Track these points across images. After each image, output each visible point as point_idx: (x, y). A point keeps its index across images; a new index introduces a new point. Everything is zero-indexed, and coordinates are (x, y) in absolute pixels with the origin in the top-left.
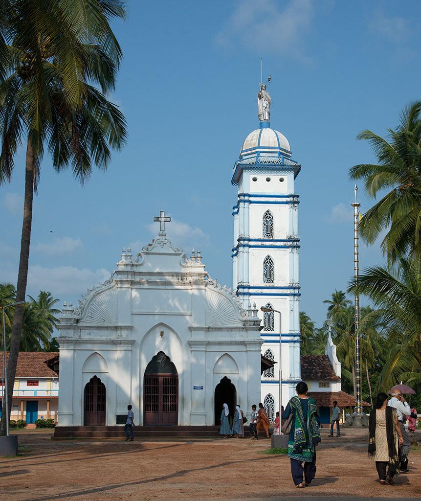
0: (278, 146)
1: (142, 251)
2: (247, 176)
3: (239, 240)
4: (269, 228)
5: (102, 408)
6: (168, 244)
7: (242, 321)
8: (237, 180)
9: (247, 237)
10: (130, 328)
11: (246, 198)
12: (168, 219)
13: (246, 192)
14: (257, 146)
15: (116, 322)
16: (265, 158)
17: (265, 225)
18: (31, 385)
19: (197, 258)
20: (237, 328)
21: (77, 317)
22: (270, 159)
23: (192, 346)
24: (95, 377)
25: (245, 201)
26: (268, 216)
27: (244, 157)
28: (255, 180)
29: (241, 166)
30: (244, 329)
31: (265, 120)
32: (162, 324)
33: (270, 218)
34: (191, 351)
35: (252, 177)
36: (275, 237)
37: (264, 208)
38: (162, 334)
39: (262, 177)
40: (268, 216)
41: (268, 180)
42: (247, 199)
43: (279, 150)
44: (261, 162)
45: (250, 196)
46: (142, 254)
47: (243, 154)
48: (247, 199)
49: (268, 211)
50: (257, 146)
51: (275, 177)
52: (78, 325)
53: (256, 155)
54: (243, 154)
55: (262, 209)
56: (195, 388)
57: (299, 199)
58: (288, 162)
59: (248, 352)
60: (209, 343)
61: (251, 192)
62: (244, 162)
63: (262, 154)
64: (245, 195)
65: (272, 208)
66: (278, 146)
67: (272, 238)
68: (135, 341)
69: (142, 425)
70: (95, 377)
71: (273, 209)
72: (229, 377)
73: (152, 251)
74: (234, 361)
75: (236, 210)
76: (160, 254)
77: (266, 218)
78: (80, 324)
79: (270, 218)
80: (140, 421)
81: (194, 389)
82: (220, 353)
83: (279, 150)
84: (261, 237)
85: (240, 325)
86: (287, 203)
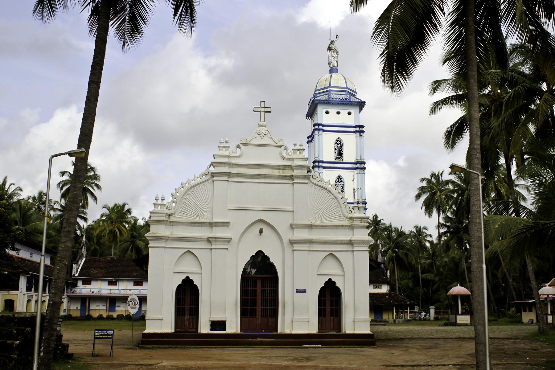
0: (345, 86)
1: (241, 142)
2: (321, 110)
3: (314, 162)
4: (339, 153)
5: (195, 312)
6: (268, 135)
7: (347, 218)
8: (311, 114)
9: (321, 159)
10: (226, 225)
11: (321, 127)
12: (269, 110)
13: (319, 122)
14: (329, 86)
15: (212, 218)
16: (334, 96)
17: (336, 150)
18: (111, 285)
19: (347, 95)
20: (342, 226)
21: (168, 212)
22: (340, 96)
23: (294, 245)
24: (188, 277)
25: (319, 130)
26: (339, 142)
27: (318, 95)
28: (327, 113)
29: (316, 101)
30: (351, 227)
31: (334, 67)
32: (261, 221)
33: (340, 144)
34: (293, 250)
35: (324, 110)
36: (345, 160)
37: (336, 136)
38: (261, 231)
39: (333, 111)
40: (339, 142)
41: (338, 113)
42: (318, 128)
43: (346, 90)
44: (333, 98)
45: (323, 126)
46: (241, 146)
47: (316, 92)
48: (318, 128)
49: (338, 139)
50: (329, 86)
51: (344, 111)
52: (169, 220)
53: (328, 93)
54: (316, 92)
55: (333, 137)
56: (297, 291)
57: (364, 129)
58: (353, 99)
59: (355, 252)
60: (312, 242)
61: (324, 123)
62: (317, 98)
63: (332, 92)
64: (319, 125)
65: (342, 136)
66: (345, 86)
67: (342, 161)
68: (231, 239)
69: (239, 332)
70: (188, 277)
71: (344, 137)
72: (334, 279)
73: (251, 142)
74: (202, 270)
75: (310, 139)
76: (259, 145)
77: (337, 144)
78: (172, 219)
79: (340, 144)
80: (237, 328)
81: (297, 292)
82: (325, 252)
83: (346, 90)
84: (333, 160)
85: (347, 222)
86: (354, 132)
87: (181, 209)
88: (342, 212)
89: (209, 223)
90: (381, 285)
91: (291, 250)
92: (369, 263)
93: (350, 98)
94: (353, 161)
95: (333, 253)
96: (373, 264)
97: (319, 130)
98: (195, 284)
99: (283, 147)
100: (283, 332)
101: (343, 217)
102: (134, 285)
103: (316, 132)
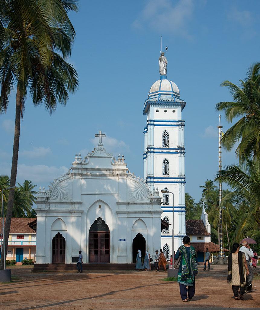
0: (171, 90)
1: (88, 156)
2: (153, 109)
5: (63, 252)
7: (149, 199)
8: (146, 111)
9: (153, 146)
10: (80, 203)
12: (104, 136)
13: (152, 119)
16: (163, 98)
17: (164, 139)
18: (19, 238)
20: (146, 203)
21: (47, 196)
22: (167, 99)
23: (119, 214)
24: (59, 233)
26: (165, 133)
27: (151, 97)
28: (157, 111)
30: (151, 204)
32: (100, 201)
33: (167, 135)
34: (118, 217)
35: (156, 109)
36: (170, 147)
37: (163, 129)
38: (100, 207)
39: (162, 109)
40: (165, 133)
41: (166, 111)
42: (152, 123)
43: (172, 93)
44: (161, 100)
45: (154, 121)
48: (152, 123)
49: (165, 131)
51: (170, 110)
52: (48, 201)
53: (158, 96)
56: (120, 240)
57: (185, 123)
58: (178, 101)
60: (129, 213)
61: (155, 119)
62: (151, 100)
63: (162, 96)
64: (151, 121)
65: (168, 129)
66: (171, 90)
67: (168, 147)
71: (169, 129)
72: (141, 233)
75: (146, 130)
76: (99, 157)
77: (165, 135)
78: (50, 201)
79: (167, 135)
80: (87, 261)
81: (120, 241)
82: (136, 218)
83: (172, 93)
84: (161, 147)
85: (148, 201)
86: (177, 125)
87: (55, 195)
88: (146, 195)
89: (71, 202)
90: (203, 237)
91: (117, 216)
92: (162, 224)
93: (175, 99)
94: (176, 147)
95: (141, 218)
96: (164, 224)
97: (151, 125)
98: (143, 238)
99: (112, 158)
100: (113, 263)
101: (147, 198)
102: (17, 238)
103: (149, 126)
